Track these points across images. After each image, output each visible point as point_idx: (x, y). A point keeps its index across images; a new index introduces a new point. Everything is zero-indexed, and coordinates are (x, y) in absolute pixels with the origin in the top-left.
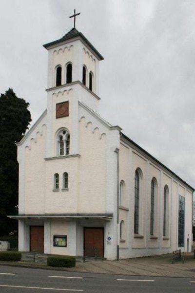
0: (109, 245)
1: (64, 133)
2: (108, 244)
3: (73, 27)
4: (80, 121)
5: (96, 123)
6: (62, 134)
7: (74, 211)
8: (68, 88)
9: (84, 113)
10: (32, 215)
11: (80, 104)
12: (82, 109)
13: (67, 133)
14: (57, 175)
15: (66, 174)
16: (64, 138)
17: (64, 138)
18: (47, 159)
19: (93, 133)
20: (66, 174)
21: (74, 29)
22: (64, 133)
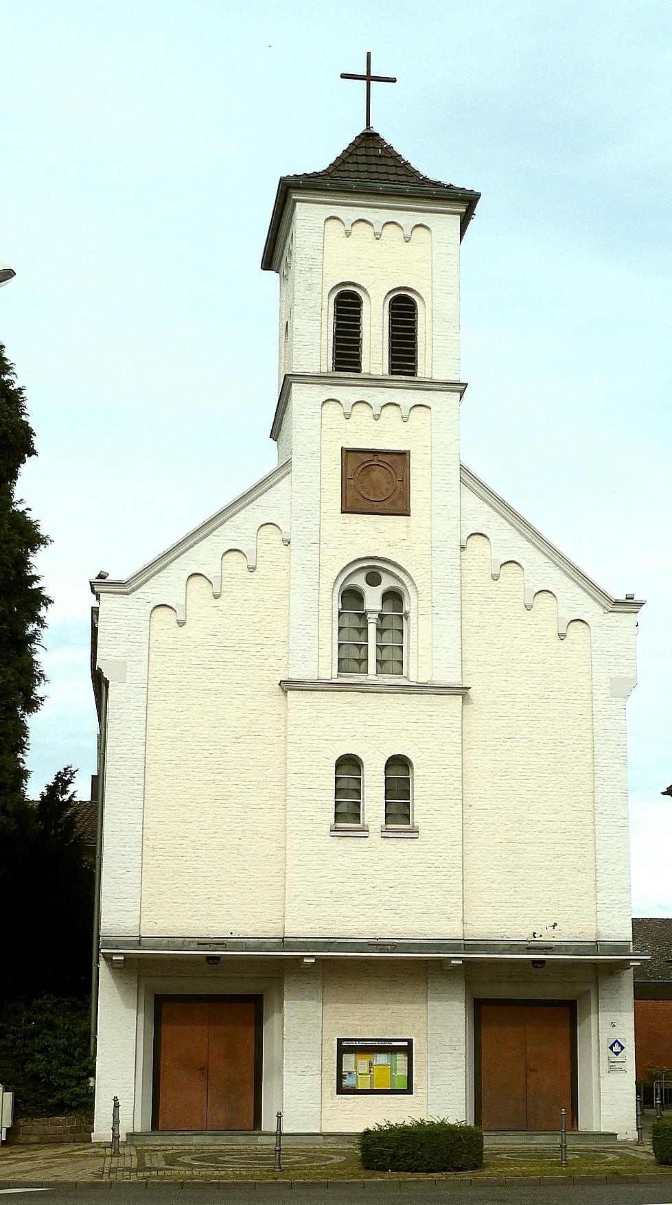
0: (613, 1076)
1: (373, 579)
2: (612, 1069)
3: (361, 128)
4: (463, 548)
5: (540, 571)
6: (360, 581)
7: (447, 928)
8: (378, 396)
9: (481, 516)
10: (221, 944)
11: (467, 477)
12: (472, 501)
13: (387, 583)
14: (349, 764)
15: (398, 764)
16: (373, 600)
17: (373, 600)
18: (287, 686)
19: (287, 543)
20: (398, 764)
21: (369, 138)
22: (373, 579)
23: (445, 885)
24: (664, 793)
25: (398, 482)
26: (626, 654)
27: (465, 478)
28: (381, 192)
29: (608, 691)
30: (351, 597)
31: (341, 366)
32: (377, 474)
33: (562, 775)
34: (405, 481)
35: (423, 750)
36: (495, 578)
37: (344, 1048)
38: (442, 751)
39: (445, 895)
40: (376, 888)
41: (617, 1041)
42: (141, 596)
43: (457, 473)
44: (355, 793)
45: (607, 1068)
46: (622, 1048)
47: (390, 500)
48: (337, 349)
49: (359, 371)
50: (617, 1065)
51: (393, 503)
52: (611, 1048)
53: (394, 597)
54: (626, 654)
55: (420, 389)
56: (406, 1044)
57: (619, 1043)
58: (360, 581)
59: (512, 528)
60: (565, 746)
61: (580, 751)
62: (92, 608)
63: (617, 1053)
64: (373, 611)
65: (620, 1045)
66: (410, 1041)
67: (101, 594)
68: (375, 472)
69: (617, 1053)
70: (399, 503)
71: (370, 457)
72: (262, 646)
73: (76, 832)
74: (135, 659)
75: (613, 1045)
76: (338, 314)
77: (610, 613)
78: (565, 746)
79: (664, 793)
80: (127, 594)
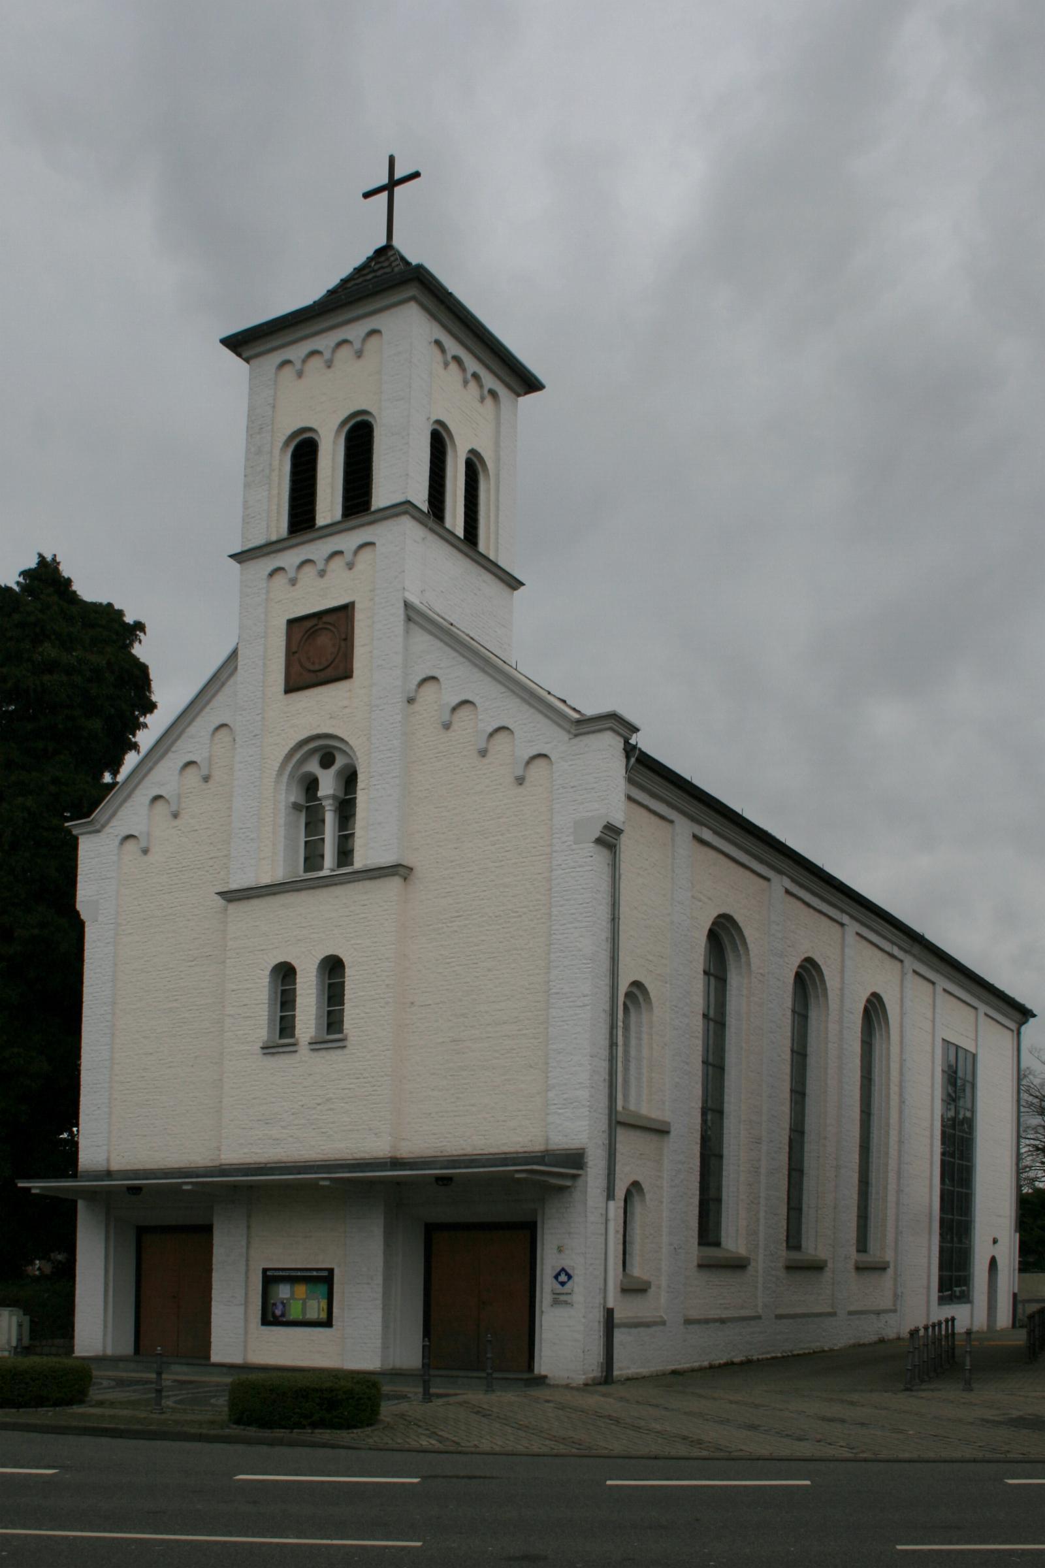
0: (560, 1311)
2: (556, 1302)
6: (313, 767)
8: (348, 542)
11: (413, 615)
12: (422, 640)
13: (340, 762)
14: (285, 973)
15: (333, 967)
16: (328, 785)
17: (328, 785)
18: (232, 896)
20: (333, 967)
22: (327, 761)
23: (374, 1097)
26: (595, 785)
27: (412, 615)
29: (571, 838)
33: (515, 952)
35: (355, 946)
36: (447, 726)
37: (270, 1279)
38: (375, 945)
39: (372, 1108)
40: (305, 1107)
42: (111, 831)
43: (400, 611)
52: (556, 1277)
53: (350, 779)
54: (595, 785)
56: (325, 1274)
60: (520, 916)
61: (538, 919)
62: (411, 869)
63: (563, 1284)
64: (327, 797)
69: (563, 1284)
72: (215, 860)
74: (105, 896)
75: (559, 1274)
78: (520, 916)
80: (98, 831)
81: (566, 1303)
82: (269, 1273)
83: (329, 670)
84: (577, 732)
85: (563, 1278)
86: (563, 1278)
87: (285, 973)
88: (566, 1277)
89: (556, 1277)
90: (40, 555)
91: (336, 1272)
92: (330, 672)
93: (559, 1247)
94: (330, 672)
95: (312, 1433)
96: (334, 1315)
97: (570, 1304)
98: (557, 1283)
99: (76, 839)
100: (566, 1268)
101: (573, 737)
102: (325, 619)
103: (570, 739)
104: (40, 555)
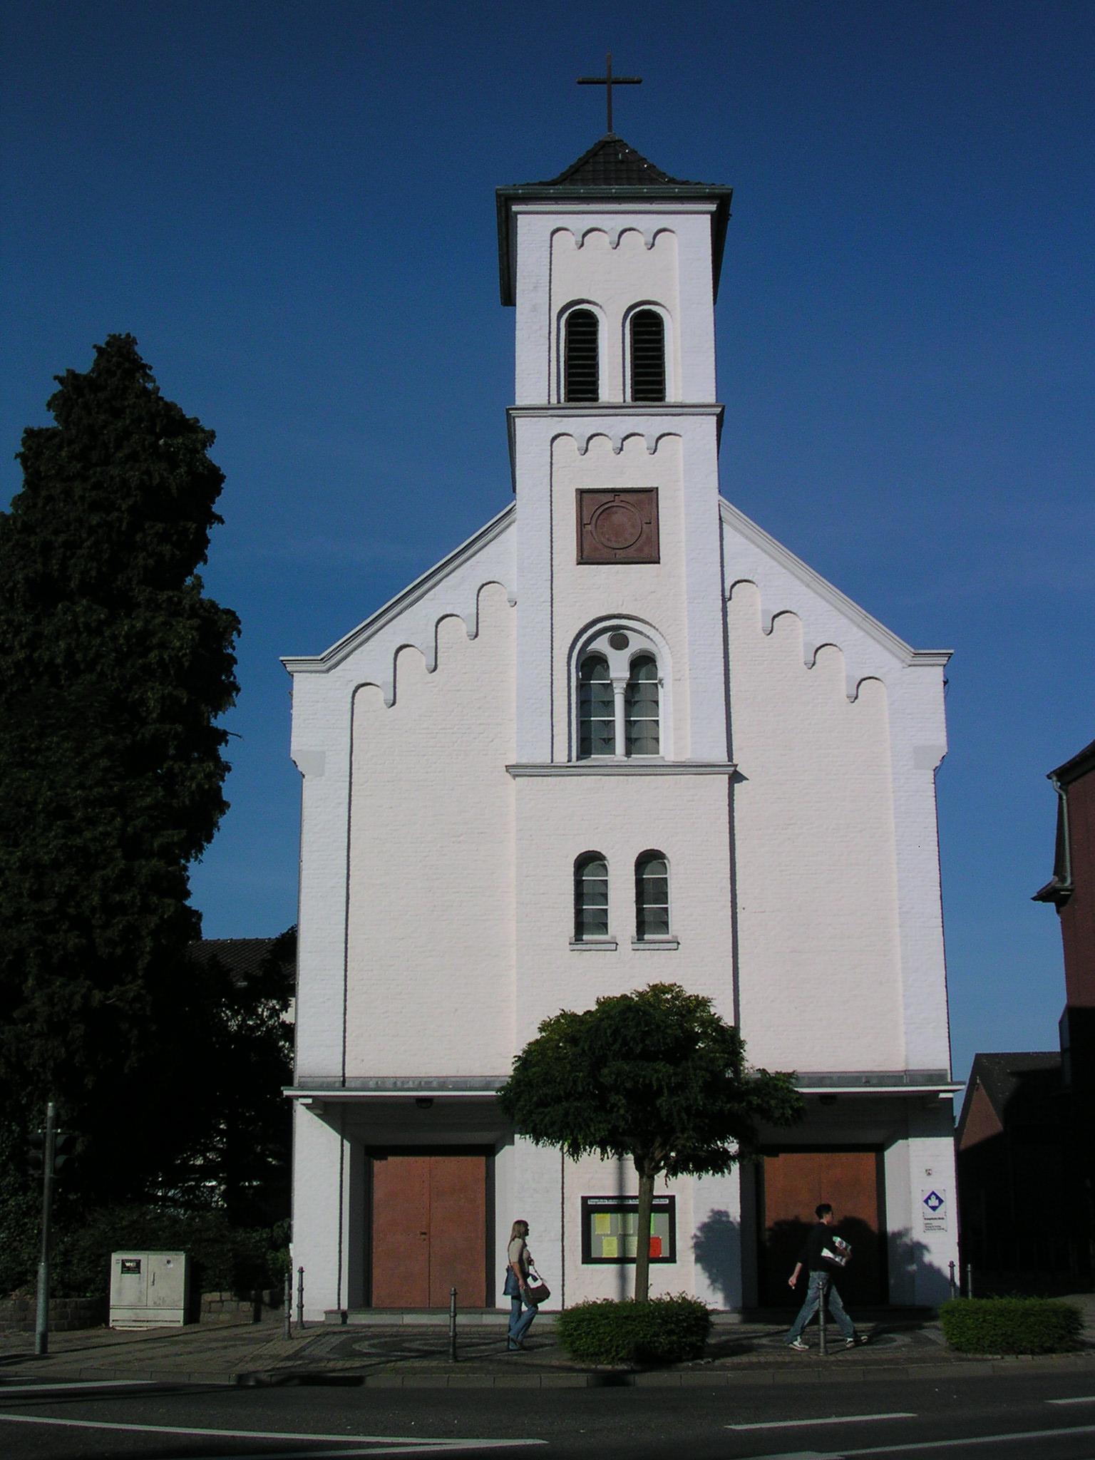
14: (589, 862)
15: (649, 860)
20: (649, 860)
22: (619, 642)
24: (1034, 899)
25: (645, 526)
28: (583, 195)
30: (591, 665)
31: (580, 396)
32: (618, 518)
34: (654, 522)
41: (933, 1193)
44: (603, 899)
45: (922, 1227)
46: (941, 1201)
47: (634, 547)
48: (636, 394)
49: (596, 399)
50: (935, 1223)
51: (640, 550)
52: (926, 1201)
53: (644, 663)
55: (667, 415)
56: (667, 1201)
57: (935, 1194)
58: (602, 645)
59: (784, 571)
63: (934, 1208)
64: (619, 679)
65: (937, 1197)
66: (672, 1198)
67: (295, 674)
68: (616, 515)
69: (934, 1208)
70: (646, 550)
71: (610, 497)
73: (611, 1151)
75: (929, 1198)
76: (636, 346)
77: (910, 668)
79: (1034, 899)
81: (940, 1228)
82: (590, 1202)
83: (632, 550)
84: (913, 663)
85: (934, 1202)
86: (934, 1202)
87: (589, 862)
88: (937, 1201)
89: (926, 1201)
90: (95, 346)
91: (677, 1199)
92: (631, 552)
93: (926, 1171)
94: (631, 552)
95: (1002, 1358)
96: (677, 1248)
97: (943, 1229)
98: (928, 1208)
99: (291, 675)
100: (936, 1192)
101: (906, 666)
102: (623, 497)
103: (904, 668)
104: (95, 346)
